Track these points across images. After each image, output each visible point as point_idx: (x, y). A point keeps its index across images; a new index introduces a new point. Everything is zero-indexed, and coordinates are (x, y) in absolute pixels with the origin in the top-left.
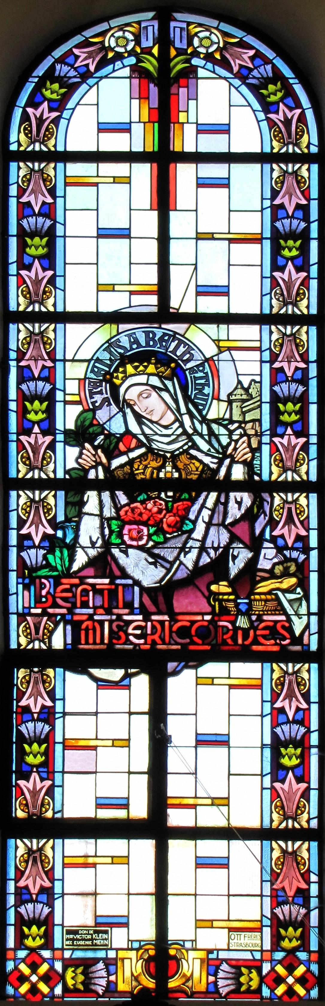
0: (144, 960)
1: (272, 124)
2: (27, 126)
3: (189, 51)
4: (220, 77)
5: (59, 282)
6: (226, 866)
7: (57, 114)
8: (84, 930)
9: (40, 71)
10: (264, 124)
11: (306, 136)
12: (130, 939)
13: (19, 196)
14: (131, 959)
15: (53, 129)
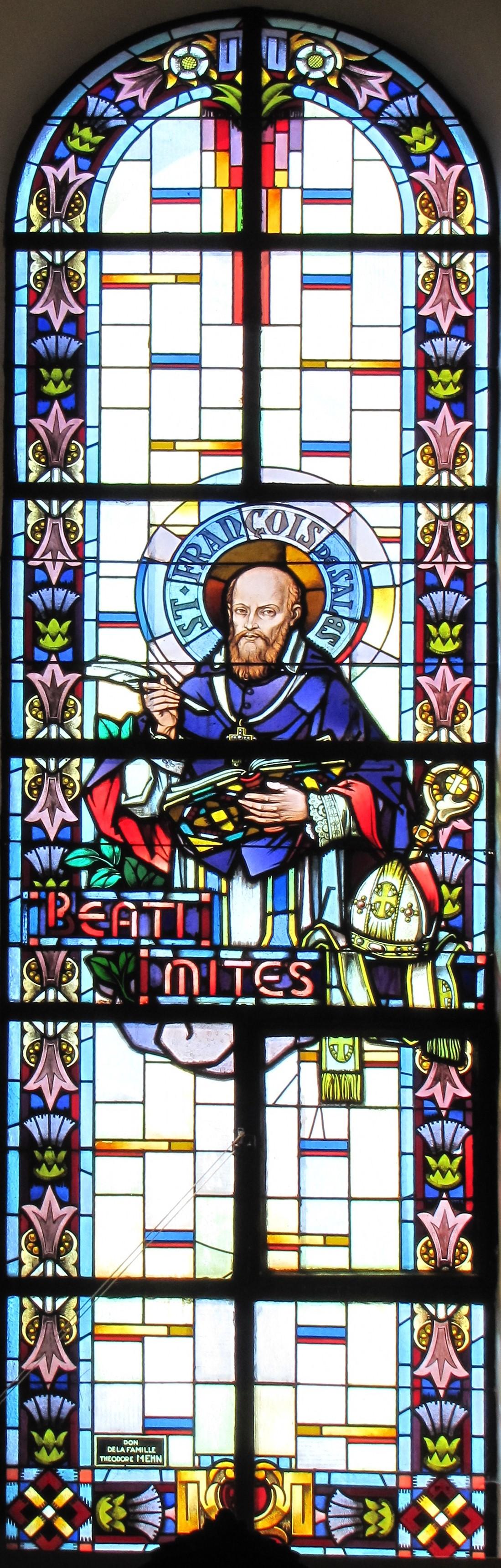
0: (219, 1484)
1: (418, 188)
2: (41, 196)
3: (290, 76)
4: (341, 117)
5: (91, 436)
6: (349, 201)
7: (89, 176)
8: (133, 1439)
9: (64, 110)
10: (407, 189)
11: (470, 206)
12: (197, 1452)
13: (31, 303)
14: (198, 1483)
15: (80, 198)
